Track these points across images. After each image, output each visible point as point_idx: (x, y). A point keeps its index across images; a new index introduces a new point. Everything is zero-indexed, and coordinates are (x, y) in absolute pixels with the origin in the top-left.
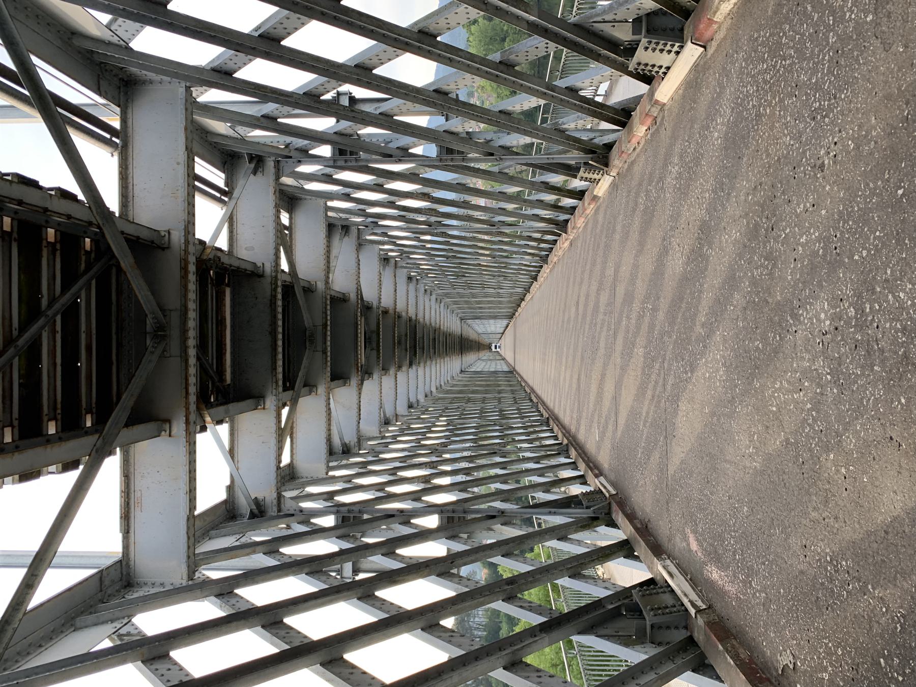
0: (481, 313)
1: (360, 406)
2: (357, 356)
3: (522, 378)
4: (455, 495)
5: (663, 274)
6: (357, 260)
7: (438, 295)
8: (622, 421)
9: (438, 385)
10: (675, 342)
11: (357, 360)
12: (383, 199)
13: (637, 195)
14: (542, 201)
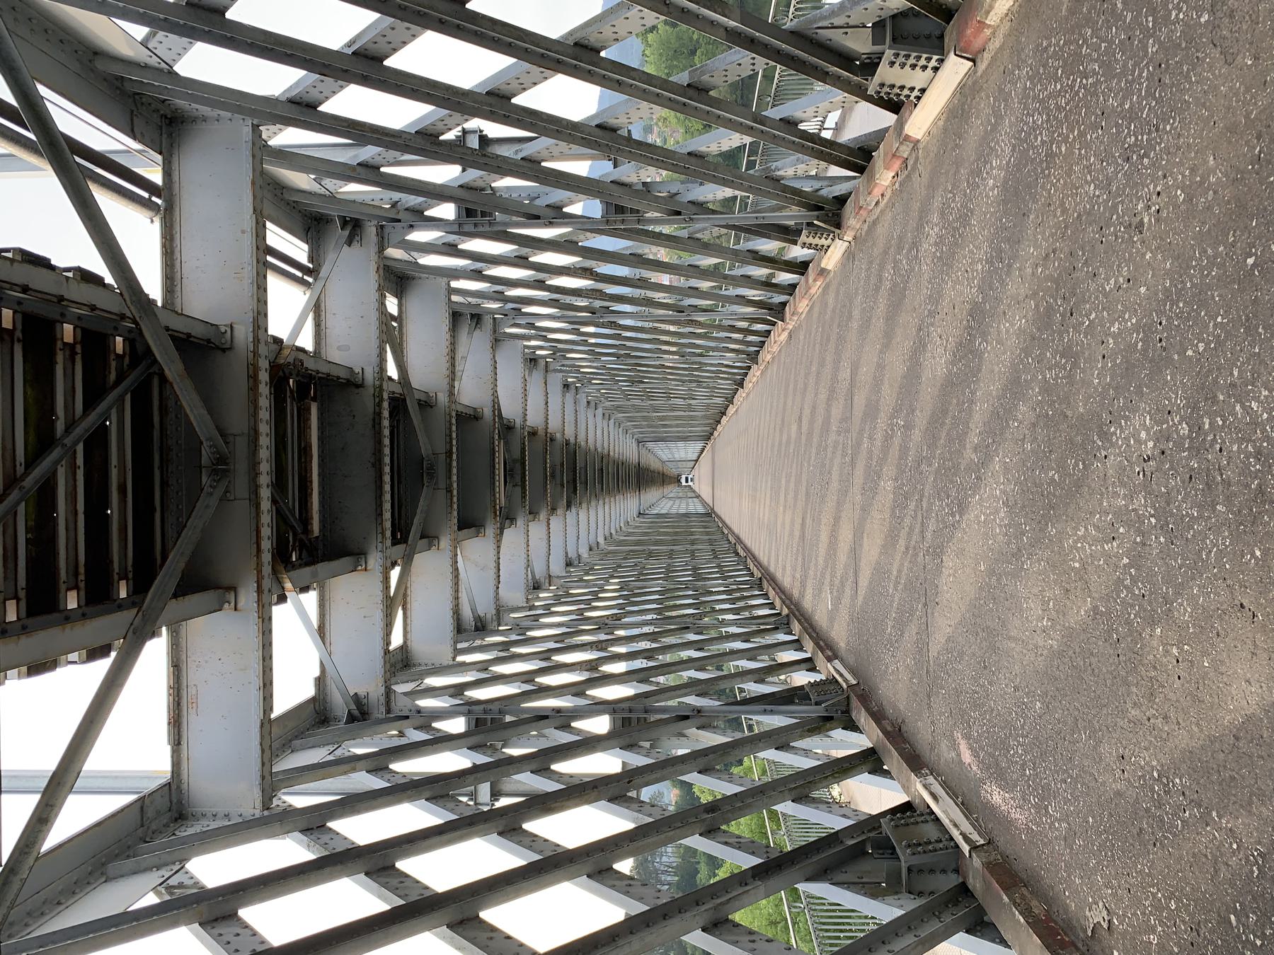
1: (499, 564)
2: (494, 495)
3: (723, 522)
4: (631, 687)
5: (919, 377)
6: (492, 362)
7: (605, 408)
8: (864, 582)
9: (607, 534)
10: (937, 471)
11: (495, 501)
12: (529, 276)
13: (882, 267)
14: (749, 277)
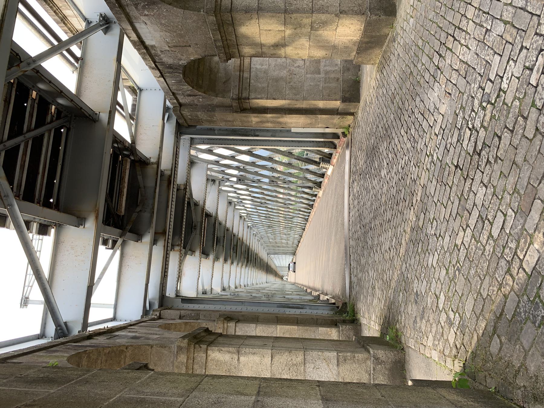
0: (279, 250)
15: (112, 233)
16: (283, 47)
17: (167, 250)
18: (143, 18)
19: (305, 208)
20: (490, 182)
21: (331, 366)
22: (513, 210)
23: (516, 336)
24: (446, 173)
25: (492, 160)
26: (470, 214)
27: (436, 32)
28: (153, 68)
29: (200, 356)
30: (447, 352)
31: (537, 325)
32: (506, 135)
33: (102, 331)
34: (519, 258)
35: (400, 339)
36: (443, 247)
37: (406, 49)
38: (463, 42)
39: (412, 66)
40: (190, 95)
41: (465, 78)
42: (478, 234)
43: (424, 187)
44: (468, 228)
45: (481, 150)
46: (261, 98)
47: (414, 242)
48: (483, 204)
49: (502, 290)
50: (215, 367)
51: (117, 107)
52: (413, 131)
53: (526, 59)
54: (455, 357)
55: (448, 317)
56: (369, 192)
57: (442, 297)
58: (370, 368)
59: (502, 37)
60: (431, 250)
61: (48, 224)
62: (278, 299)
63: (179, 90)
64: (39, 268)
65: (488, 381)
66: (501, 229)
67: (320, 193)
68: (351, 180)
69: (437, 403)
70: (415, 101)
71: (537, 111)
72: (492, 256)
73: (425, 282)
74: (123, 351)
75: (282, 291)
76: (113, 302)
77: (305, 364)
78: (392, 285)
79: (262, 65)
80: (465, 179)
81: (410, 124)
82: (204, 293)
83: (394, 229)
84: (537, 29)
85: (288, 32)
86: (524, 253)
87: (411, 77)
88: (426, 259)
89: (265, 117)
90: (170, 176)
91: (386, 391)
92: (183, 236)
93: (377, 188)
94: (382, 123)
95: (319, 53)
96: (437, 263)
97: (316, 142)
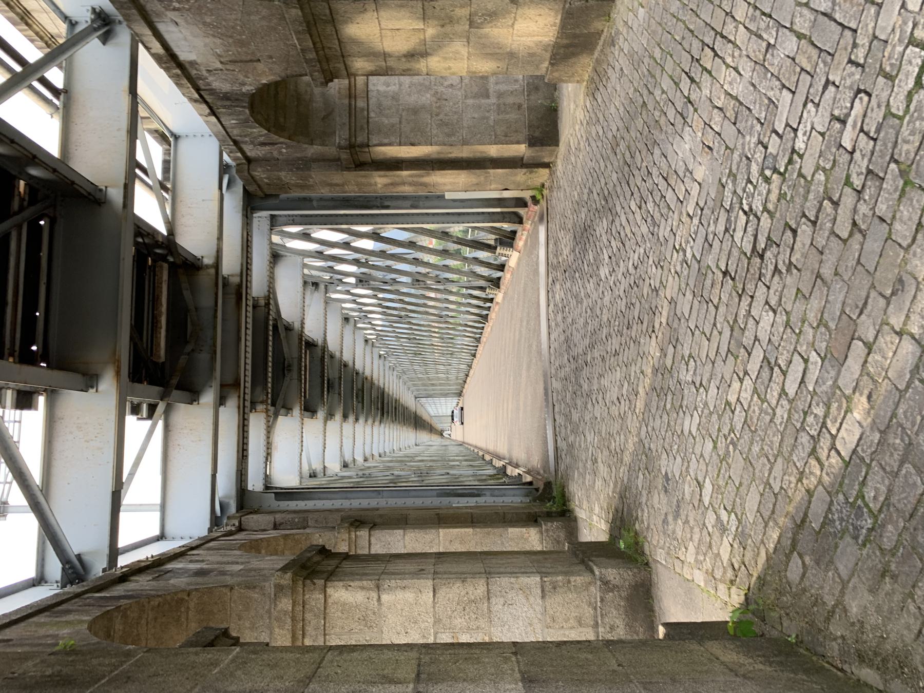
0: (433, 390)
15: (146, 393)
16: (422, 56)
17: (244, 413)
18: (171, 15)
19: (475, 322)
20: (780, 305)
21: (532, 599)
22: (819, 354)
23: (828, 558)
24: (708, 282)
25: (781, 266)
26: (749, 354)
27: (683, 38)
28: (196, 101)
29: (315, 598)
30: (718, 574)
31: (860, 542)
32: (805, 229)
33: (143, 564)
34: (829, 432)
35: (642, 547)
36: (706, 404)
37: (635, 61)
38: (729, 60)
39: (645, 92)
40: (263, 144)
41: (735, 124)
42: (762, 387)
43: (672, 302)
44: (747, 377)
45: (764, 250)
46: (390, 144)
47: (659, 391)
48: (770, 339)
49: (805, 481)
50: (340, 614)
51: (138, 171)
52: (650, 206)
53: (834, 103)
54: (732, 582)
55: (718, 517)
56: (581, 303)
57: (708, 486)
58: (596, 598)
59: (793, 59)
60: (687, 407)
61: (33, 390)
62: (437, 478)
63: (245, 136)
64: (24, 470)
65: (785, 624)
66: (801, 383)
67: (499, 297)
68: (550, 279)
69: (707, 672)
70: (652, 154)
71: (855, 194)
72: (786, 426)
73: (679, 460)
74: (182, 599)
75: (444, 460)
76: (158, 500)
77: (489, 599)
78: (625, 459)
79: (388, 86)
80: (740, 296)
81: (645, 193)
82: (313, 475)
83: (624, 368)
84: (850, 54)
85: (431, 32)
86: (838, 425)
87: (644, 113)
88: (679, 421)
89: (398, 176)
90: (240, 286)
91: (624, 655)
92: (270, 385)
93: (595, 296)
94: (598, 186)
95: (485, 66)
96: (698, 429)
97: (489, 213)
